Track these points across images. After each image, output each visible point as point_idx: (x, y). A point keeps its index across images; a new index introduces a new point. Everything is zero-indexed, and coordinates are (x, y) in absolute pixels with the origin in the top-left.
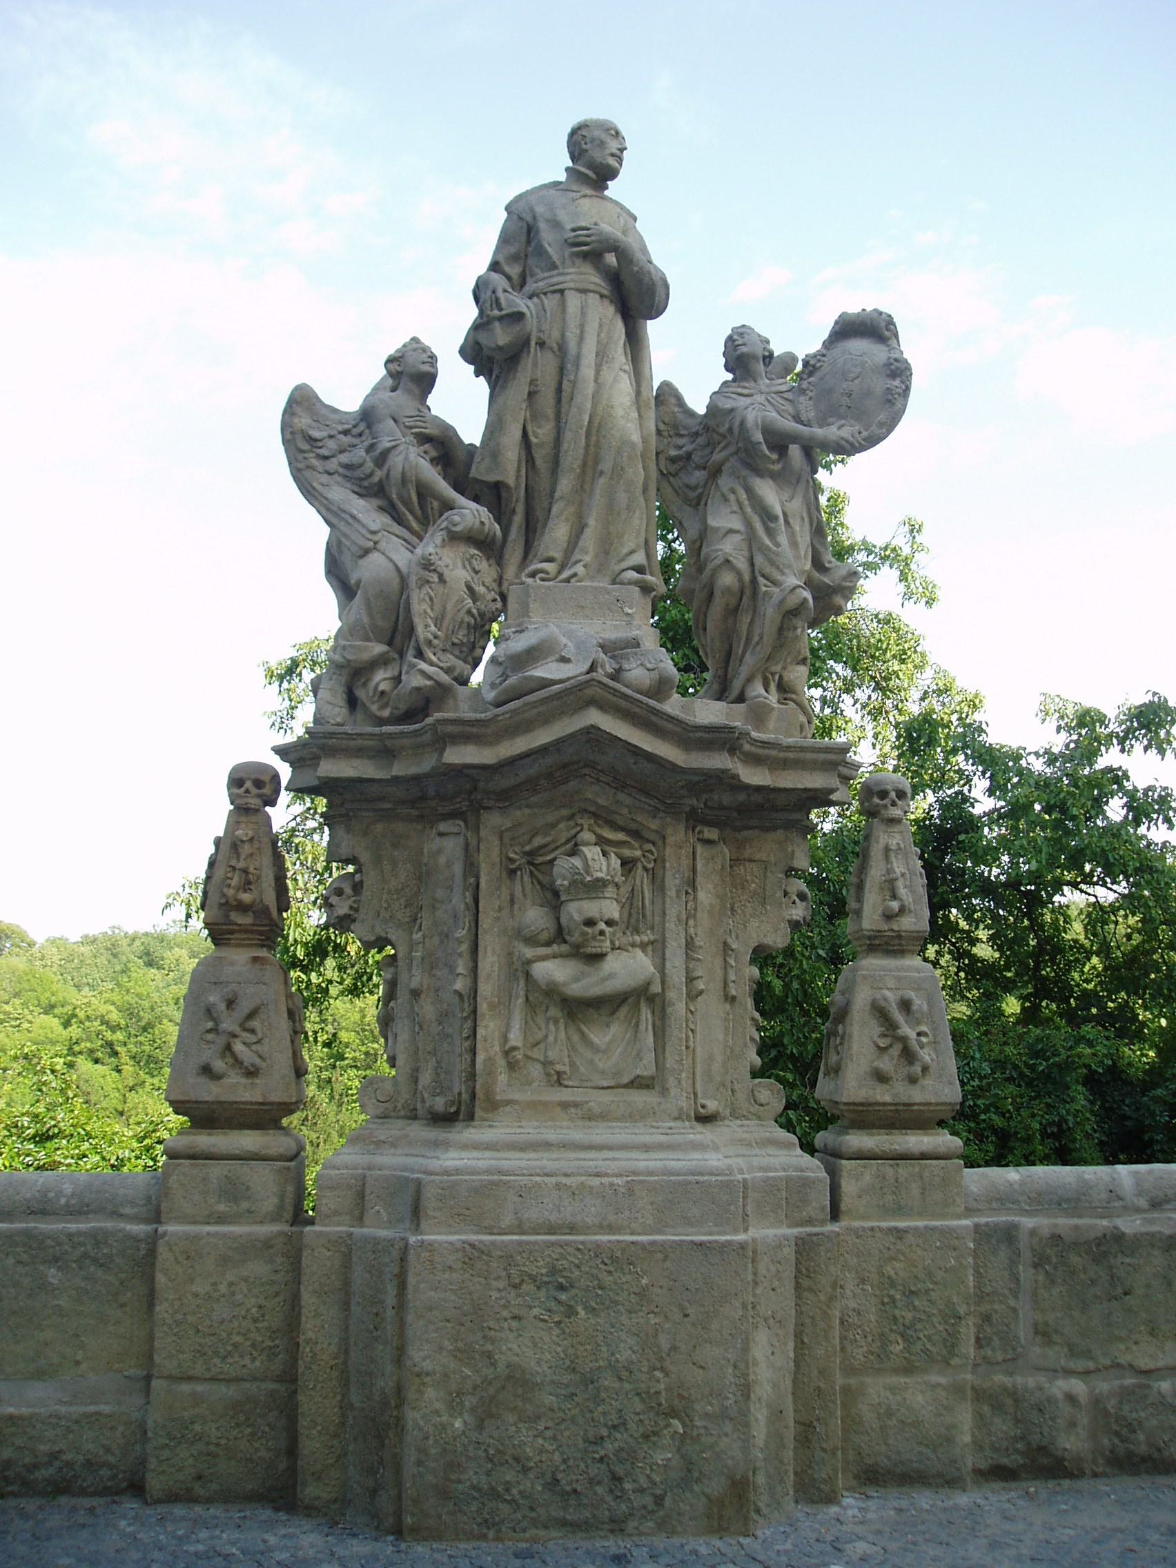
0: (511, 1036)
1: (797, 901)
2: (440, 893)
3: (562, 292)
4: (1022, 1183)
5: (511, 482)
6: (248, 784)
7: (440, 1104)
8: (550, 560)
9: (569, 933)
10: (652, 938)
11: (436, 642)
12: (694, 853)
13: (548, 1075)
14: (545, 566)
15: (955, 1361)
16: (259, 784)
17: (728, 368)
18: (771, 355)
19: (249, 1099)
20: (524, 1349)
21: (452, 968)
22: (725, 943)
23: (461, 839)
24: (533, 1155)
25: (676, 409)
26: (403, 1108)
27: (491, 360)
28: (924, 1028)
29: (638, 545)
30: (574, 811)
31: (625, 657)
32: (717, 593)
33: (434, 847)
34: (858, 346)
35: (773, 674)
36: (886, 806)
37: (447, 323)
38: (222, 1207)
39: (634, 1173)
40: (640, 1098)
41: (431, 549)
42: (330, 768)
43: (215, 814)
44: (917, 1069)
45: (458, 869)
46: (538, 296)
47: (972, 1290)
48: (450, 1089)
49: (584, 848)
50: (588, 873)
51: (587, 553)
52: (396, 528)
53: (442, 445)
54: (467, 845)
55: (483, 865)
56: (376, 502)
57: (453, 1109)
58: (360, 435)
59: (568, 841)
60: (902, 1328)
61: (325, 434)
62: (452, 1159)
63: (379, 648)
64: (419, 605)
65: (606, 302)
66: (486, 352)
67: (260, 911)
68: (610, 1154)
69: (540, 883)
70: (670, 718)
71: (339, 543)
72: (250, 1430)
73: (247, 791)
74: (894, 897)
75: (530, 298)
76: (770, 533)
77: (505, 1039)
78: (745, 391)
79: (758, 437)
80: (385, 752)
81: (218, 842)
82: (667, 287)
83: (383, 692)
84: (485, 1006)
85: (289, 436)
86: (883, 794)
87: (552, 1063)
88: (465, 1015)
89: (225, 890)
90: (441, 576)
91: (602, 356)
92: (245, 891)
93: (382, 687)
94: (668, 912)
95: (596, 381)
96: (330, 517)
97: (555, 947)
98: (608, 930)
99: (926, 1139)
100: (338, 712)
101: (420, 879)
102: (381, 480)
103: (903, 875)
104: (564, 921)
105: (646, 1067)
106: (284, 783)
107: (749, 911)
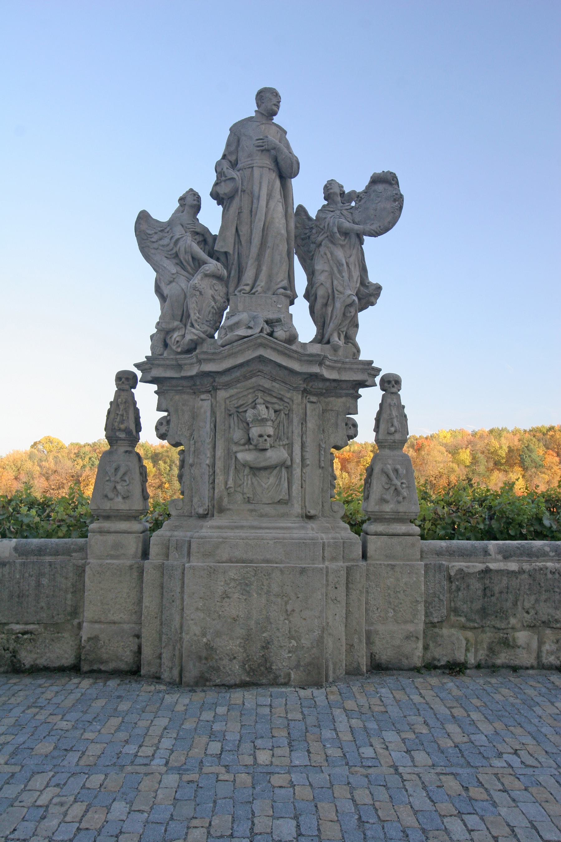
0: (229, 483)
1: (352, 427)
3: (253, 167)
4: (447, 547)
5: (231, 252)
6: (123, 380)
7: (201, 511)
8: (247, 285)
9: (253, 440)
10: (287, 442)
11: (199, 320)
12: (306, 407)
13: (244, 498)
14: (245, 287)
15: (416, 621)
16: (127, 379)
17: (326, 199)
18: (344, 192)
21: (206, 455)
22: (320, 445)
23: (210, 401)
24: (238, 531)
25: (304, 217)
27: (223, 199)
28: (404, 481)
31: (276, 326)
32: (318, 297)
34: (380, 187)
35: (342, 332)
36: (390, 387)
37: (205, 183)
38: (112, 553)
39: (278, 539)
40: (282, 509)
41: (196, 281)
42: (156, 373)
43: (110, 391)
44: (400, 499)
45: (209, 414)
46: (242, 170)
47: (423, 591)
48: (205, 504)
49: (258, 406)
50: (259, 416)
51: (262, 282)
52: (183, 272)
53: (203, 236)
55: (218, 412)
56: (175, 261)
57: (206, 513)
58: (168, 232)
59: (253, 402)
61: (153, 232)
62: (205, 532)
63: (176, 323)
64: (192, 305)
65: (272, 172)
66: (221, 196)
67: (127, 431)
68: (268, 531)
69: (241, 420)
70: (296, 352)
71: (160, 279)
72: (123, 643)
73: (123, 383)
74: (392, 425)
75: (238, 171)
76: (340, 272)
77: (226, 483)
78: (332, 209)
79: (336, 230)
80: (180, 367)
81: (111, 403)
82: (298, 164)
83: (178, 342)
84: (218, 470)
85: (137, 233)
86: (389, 382)
87: (245, 494)
90: (201, 293)
91: (270, 196)
93: (177, 339)
95: (267, 207)
96: (155, 268)
97: (247, 446)
98: (268, 439)
99: (404, 528)
100: (160, 349)
103: (397, 416)
104: (250, 435)
105: (283, 495)
106: (139, 379)
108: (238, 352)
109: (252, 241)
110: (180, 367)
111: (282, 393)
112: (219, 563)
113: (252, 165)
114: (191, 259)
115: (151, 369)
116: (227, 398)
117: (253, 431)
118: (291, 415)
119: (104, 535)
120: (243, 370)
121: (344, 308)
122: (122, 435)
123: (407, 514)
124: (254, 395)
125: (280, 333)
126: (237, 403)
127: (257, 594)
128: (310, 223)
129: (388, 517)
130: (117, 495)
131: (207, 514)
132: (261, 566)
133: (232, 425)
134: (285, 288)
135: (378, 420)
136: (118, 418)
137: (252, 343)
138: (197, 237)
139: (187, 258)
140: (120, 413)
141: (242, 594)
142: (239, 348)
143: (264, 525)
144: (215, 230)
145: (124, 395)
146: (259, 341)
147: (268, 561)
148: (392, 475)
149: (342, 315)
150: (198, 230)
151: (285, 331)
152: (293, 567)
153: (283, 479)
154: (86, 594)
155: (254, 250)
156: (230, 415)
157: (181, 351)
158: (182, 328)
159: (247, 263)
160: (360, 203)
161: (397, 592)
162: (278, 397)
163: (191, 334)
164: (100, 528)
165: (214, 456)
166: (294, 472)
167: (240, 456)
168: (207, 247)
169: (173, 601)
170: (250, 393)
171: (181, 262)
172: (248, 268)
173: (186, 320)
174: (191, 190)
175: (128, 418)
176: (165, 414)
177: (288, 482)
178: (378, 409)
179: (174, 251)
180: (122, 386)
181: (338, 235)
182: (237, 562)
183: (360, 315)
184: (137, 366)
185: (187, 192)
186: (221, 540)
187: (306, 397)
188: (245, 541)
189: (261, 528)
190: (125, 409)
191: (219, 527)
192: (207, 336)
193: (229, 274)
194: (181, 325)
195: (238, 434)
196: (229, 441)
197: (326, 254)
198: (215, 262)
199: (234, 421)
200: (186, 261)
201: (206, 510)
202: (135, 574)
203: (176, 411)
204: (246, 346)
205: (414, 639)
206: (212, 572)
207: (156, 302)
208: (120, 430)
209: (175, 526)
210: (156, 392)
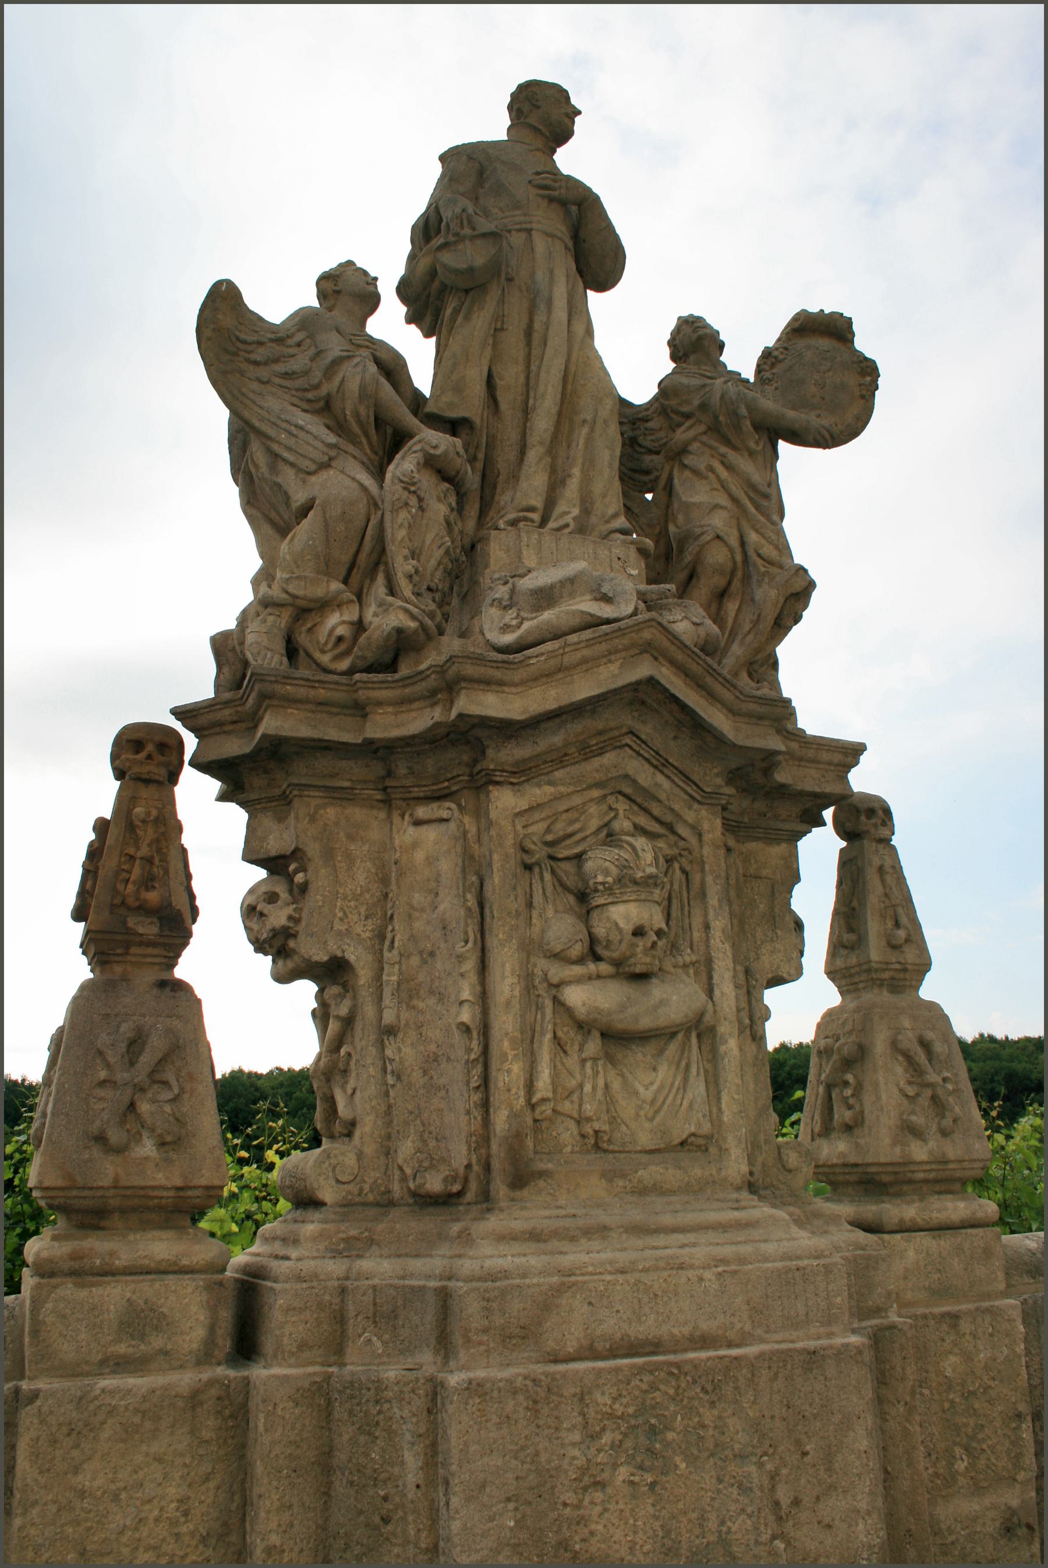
2: (418, 898)
3: (529, 231)
6: (150, 748)
7: (434, 1184)
13: (583, 1136)
19: (163, 1182)
20: (612, 1530)
26: (371, 1190)
30: (606, 791)
38: (122, 1349)
39: (724, 1261)
57: (456, 1188)
59: (599, 829)
60: (965, 1440)
63: (336, 586)
68: (681, 1238)
73: (149, 757)
77: (530, 1087)
83: (340, 639)
87: (589, 1119)
88: (473, 1056)
89: (120, 887)
92: (147, 889)
93: (341, 631)
94: (712, 924)
102: (329, 395)
107: (759, 934)
108: (575, 666)
110: (360, 710)
111: (677, 807)
112: (556, 1361)
113: (528, 226)
116: (521, 814)
119: (93, 1285)
120: (576, 728)
121: (782, 600)
126: (548, 830)
129: (920, 1176)
130: (137, 1138)
131: (460, 1194)
132: (691, 1361)
137: (626, 641)
139: (363, 411)
140: (144, 851)
141: (641, 1467)
142: (586, 652)
143: (667, 1220)
146: (647, 635)
147: (704, 1341)
148: (921, 1057)
151: (695, 624)
152: (782, 1352)
155: (542, 424)
156: (528, 867)
158: (352, 601)
161: (970, 1393)
162: (664, 818)
163: (387, 616)
164: (75, 1256)
165: (484, 998)
166: (722, 1048)
169: (386, 1520)
170: (591, 800)
175: (166, 871)
180: (146, 769)
182: (613, 1353)
184: (179, 713)
186: (555, 1279)
188: (631, 1278)
189: (658, 1230)
190: (158, 841)
191: (535, 1236)
194: (349, 595)
196: (529, 948)
199: (543, 884)
203: (329, 854)
204: (604, 647)
205: (1025, 1530)
206: (539, 1397)
208: (143, 909)
209: (346, 1240)
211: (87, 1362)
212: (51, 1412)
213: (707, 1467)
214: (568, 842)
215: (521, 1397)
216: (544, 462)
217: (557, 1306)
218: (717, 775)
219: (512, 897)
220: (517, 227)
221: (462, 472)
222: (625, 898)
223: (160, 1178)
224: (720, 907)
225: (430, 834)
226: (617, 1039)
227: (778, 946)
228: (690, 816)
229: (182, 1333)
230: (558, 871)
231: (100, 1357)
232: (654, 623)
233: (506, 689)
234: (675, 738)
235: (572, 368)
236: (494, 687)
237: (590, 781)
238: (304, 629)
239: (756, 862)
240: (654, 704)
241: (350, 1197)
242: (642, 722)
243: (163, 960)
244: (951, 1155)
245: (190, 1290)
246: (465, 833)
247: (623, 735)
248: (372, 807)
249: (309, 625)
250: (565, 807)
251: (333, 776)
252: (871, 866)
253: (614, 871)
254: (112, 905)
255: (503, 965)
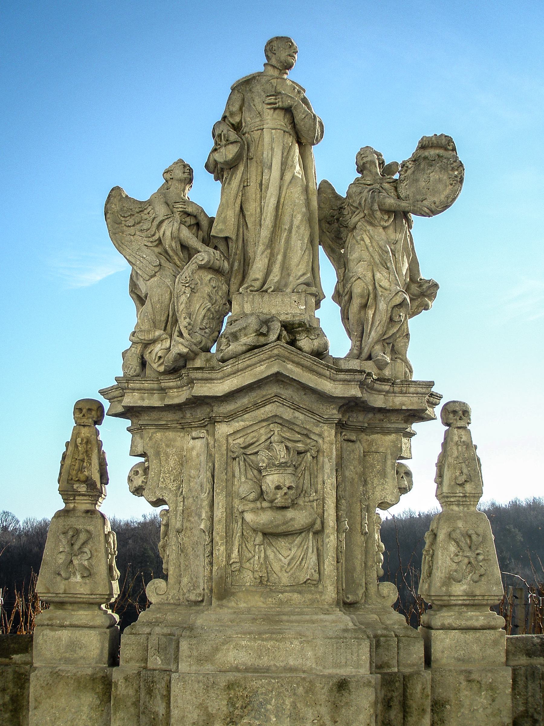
0: (233, 556)
2: (193, 472)
5: (234, 237)
7: (193, 597)
10: (315, 498)
21: (200, 516)
26: (172, 598)
29: (307, 270)
33: (190, 445)
37: (198, 150)
43: (65, 427)
48: (198, 587)
53: (196, 221)
54: (208, 444)
57: (200, 599)
69: (250, 465)
73: (84, 415)
77: (229, 556)
83: (160, 357)
86: (455, 412)
101: (182, 464)
104: (264, 488)
106: (106, 412)
109: (263, 222)
113: (262, 127)
114: (179, 247)
115: (123, 396)
117: (268, 481)
118: (321, 459)
122: (83, 488)
123: (486, 598)
124: (268, 430)
125: (305, 343)
127: (276, 717)
128: (339, 202)
131: (202, 601)
133: (237, 473)
134: (308, 284)
135: (440, 466)
136: (77, 465)
138: (188, 219)
139: (174, 244)
140: (81, 457)
144: (212, 211)
145: (85, 432)
149: (388, 320)
150: (190, 210)
153: (310, 550)
154: (30, 713)
155: (265, 233)
156: (234, 459)
157: (165, 370)
159: (255, 253)
160: (406, 175)
161: (474, 710)
165: (212, 518)
167: (249, 517)
168: (200, 233)
171: (166, 252)
172: (258, 259)
173: (172, 329)
174: (181, 161)
175: (90, 464)
176: (142, 459)
177: (318, 555)
178: (439, 450)
179: (156, 237)
181: (379, 213)
183: (410, 321)
184: (103, 392)
185: (176, 163)
187: (341, 433)
192: (201, 349)
193: (232, 266)
195: (244, 486)
197: (363, 240)
198: (211, 250)
199: (237, 468)
200: (173, 250)
201: (200, 594)
202: (100, 688)
203: (157, 454)
207: (131, 305)
210: (129, 429)
211: (54, 659)
212: (41, 676)
213: (286, 721)
214: (253, 446)
215: (201, 684)
216: (266, 253)
217: (222, 650)
218: (333, 409)
219: (224, 473)
220: (256, 128)
221: (222, 267)
222: (272, 473)
223: (82, 590)
224: (331, 473)
225: (199, 443)
226: (270, 535)
227: (386, 487)
228: (317, 430)
229: (90, 651)
230: (248, 460)
231: (59, 657)
232: (278, 346)
233: (215, 381)
234: (305, 394)
235: (282, 200)
236: (209, 381)
237: (260, 419)
238: (147, 352)
239: (376, 445)
240: (288, 381)
241: (162, 601)
242: (286, 389)
243: (90, 501)
244: (478, 593)
245: (93, 635)
246: (208, 444)
247: (273, 397)
248: (177, 431)
249: (149, 351)
250: (251, 431)
251: (159, 419)
252: (452, 442)
253: (266, 461)
254: (68, 480)
255: (218, 504)
